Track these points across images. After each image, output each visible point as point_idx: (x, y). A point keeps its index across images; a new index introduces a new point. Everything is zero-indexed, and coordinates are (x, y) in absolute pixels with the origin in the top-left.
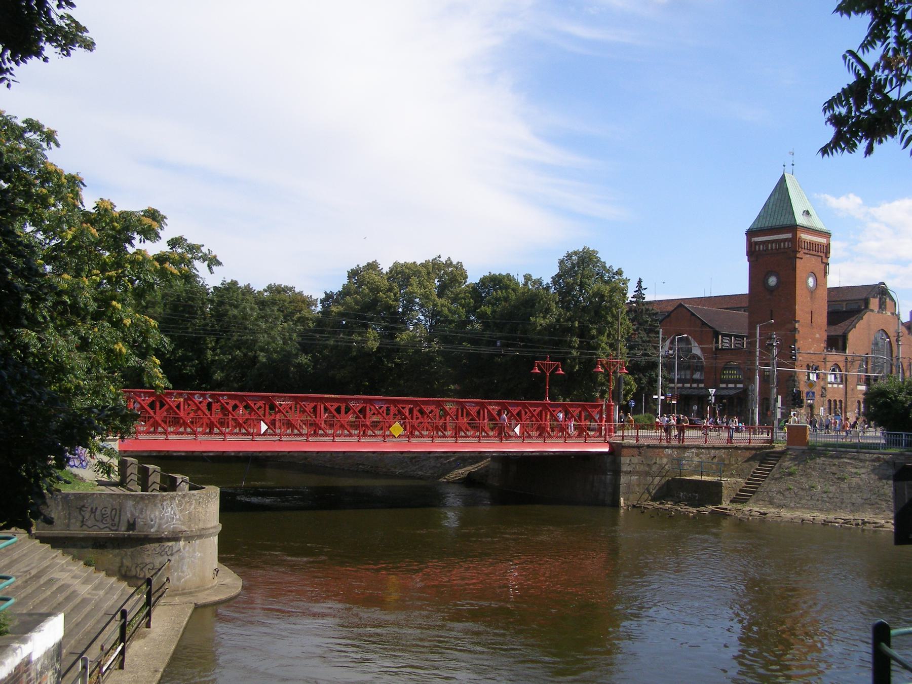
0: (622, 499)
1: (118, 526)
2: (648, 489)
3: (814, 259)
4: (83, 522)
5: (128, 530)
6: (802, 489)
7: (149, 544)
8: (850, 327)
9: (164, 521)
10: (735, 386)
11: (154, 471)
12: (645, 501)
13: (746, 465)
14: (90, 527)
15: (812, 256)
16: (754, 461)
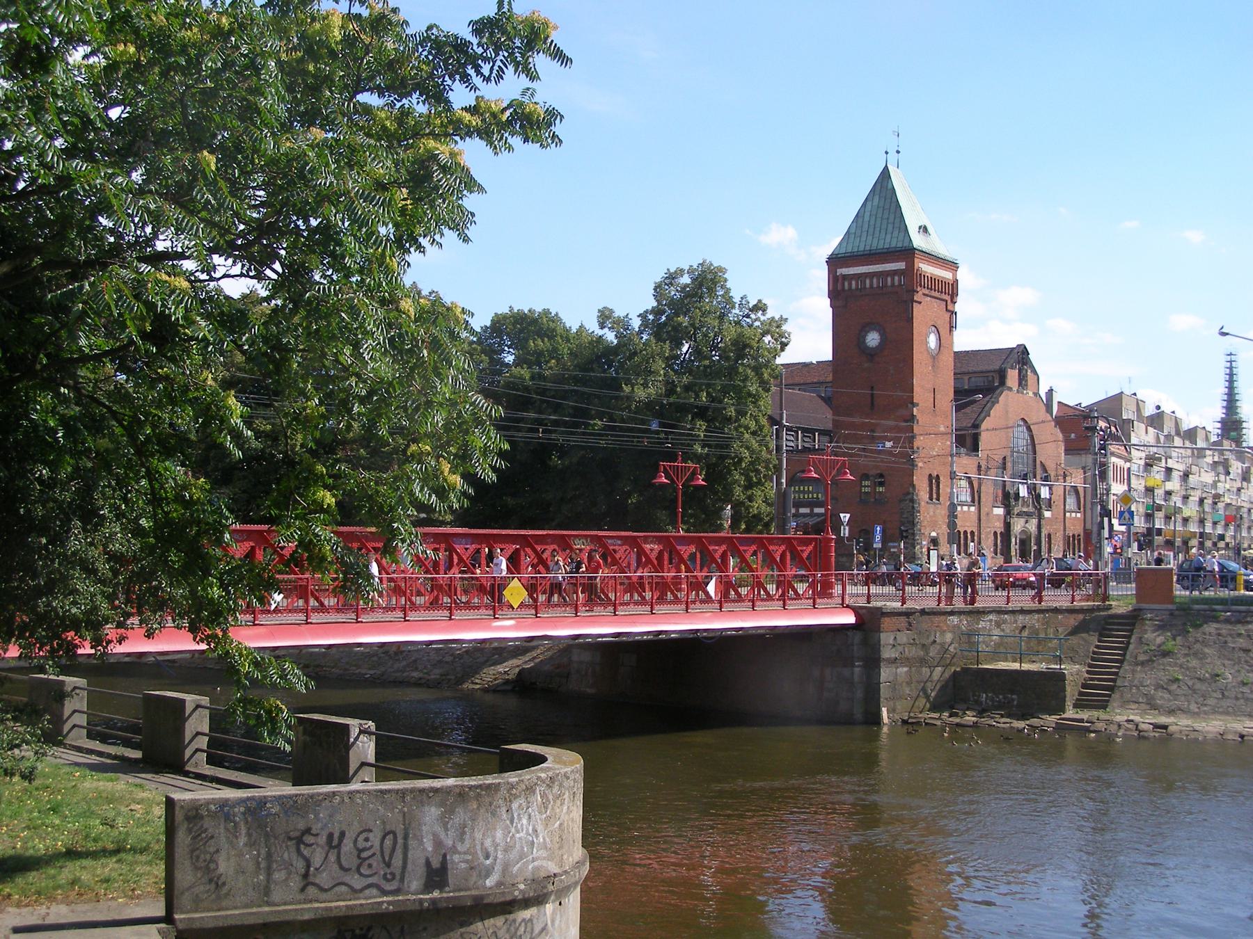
0: (884, 711)
1: (402, 880)
2: (924, 690)
3: (936, 303)
4: (306, 876)
5: (428, 887)
6: (1199, 679)
7: (482, 920)
8: (983, 415)
9: (513, 855)
10: (812, 510)
11: (198, 706)
12: (921, 712)
13: (1074, 640)
14: (326, 890)
15: (933, 300)
16: (1088, 632)
